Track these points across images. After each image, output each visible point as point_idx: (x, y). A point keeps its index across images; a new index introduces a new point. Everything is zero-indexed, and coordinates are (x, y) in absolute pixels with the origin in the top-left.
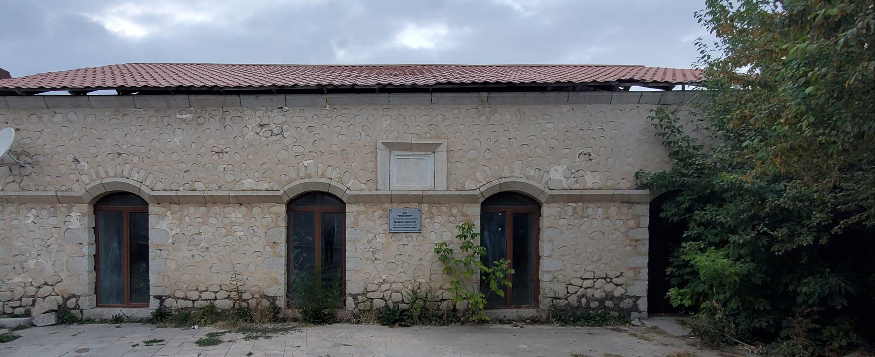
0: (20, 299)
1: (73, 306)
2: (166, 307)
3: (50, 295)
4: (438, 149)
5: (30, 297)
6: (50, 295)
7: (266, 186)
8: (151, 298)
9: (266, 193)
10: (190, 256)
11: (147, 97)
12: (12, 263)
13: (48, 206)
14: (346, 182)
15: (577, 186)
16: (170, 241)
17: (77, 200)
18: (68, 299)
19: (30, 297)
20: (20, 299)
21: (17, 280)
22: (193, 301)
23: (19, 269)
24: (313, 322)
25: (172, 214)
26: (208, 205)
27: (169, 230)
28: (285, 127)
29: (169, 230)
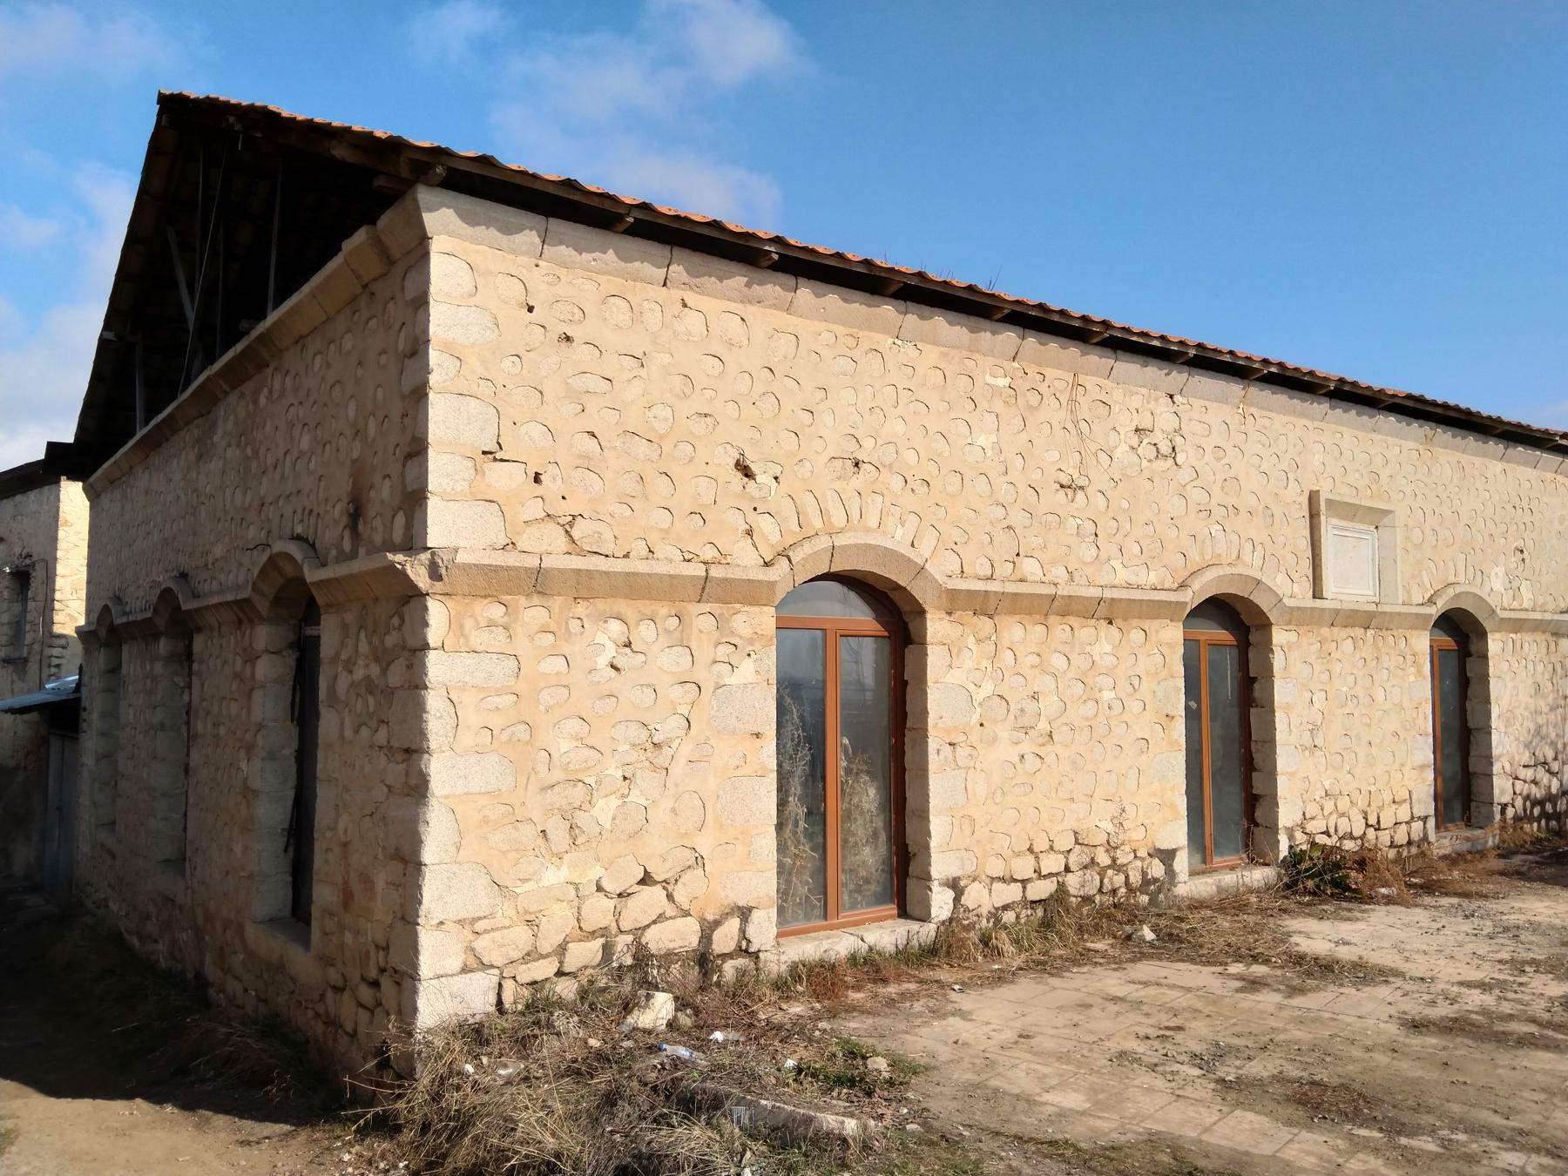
0: (562, 949)
1: (729, 947)
2: (967, 910)
3: (661, 918)
4: (1386, 520)
5: (593, 935)
6: (661, 918)
7: (1153, 578)
8: (935, 886)
9: (1157, 596)
10: (1016, 759)
11: (806, 294)
12: (537, 815)
13: (663, 610)
14: (1495, 589)
15: (1515, 605)
16: (975, 719)
17: (748, 593)
18: (717, 923)
19: (593, 935)
20: (562, 949)
21: (554, 876)
22: (1024, 882)
23: (559, 835)
24: (1542, 879)
25: (979, 641)
26: (1119, 622)
27: (971, 687)
28: (1178, 441)
29: (971, 687)
